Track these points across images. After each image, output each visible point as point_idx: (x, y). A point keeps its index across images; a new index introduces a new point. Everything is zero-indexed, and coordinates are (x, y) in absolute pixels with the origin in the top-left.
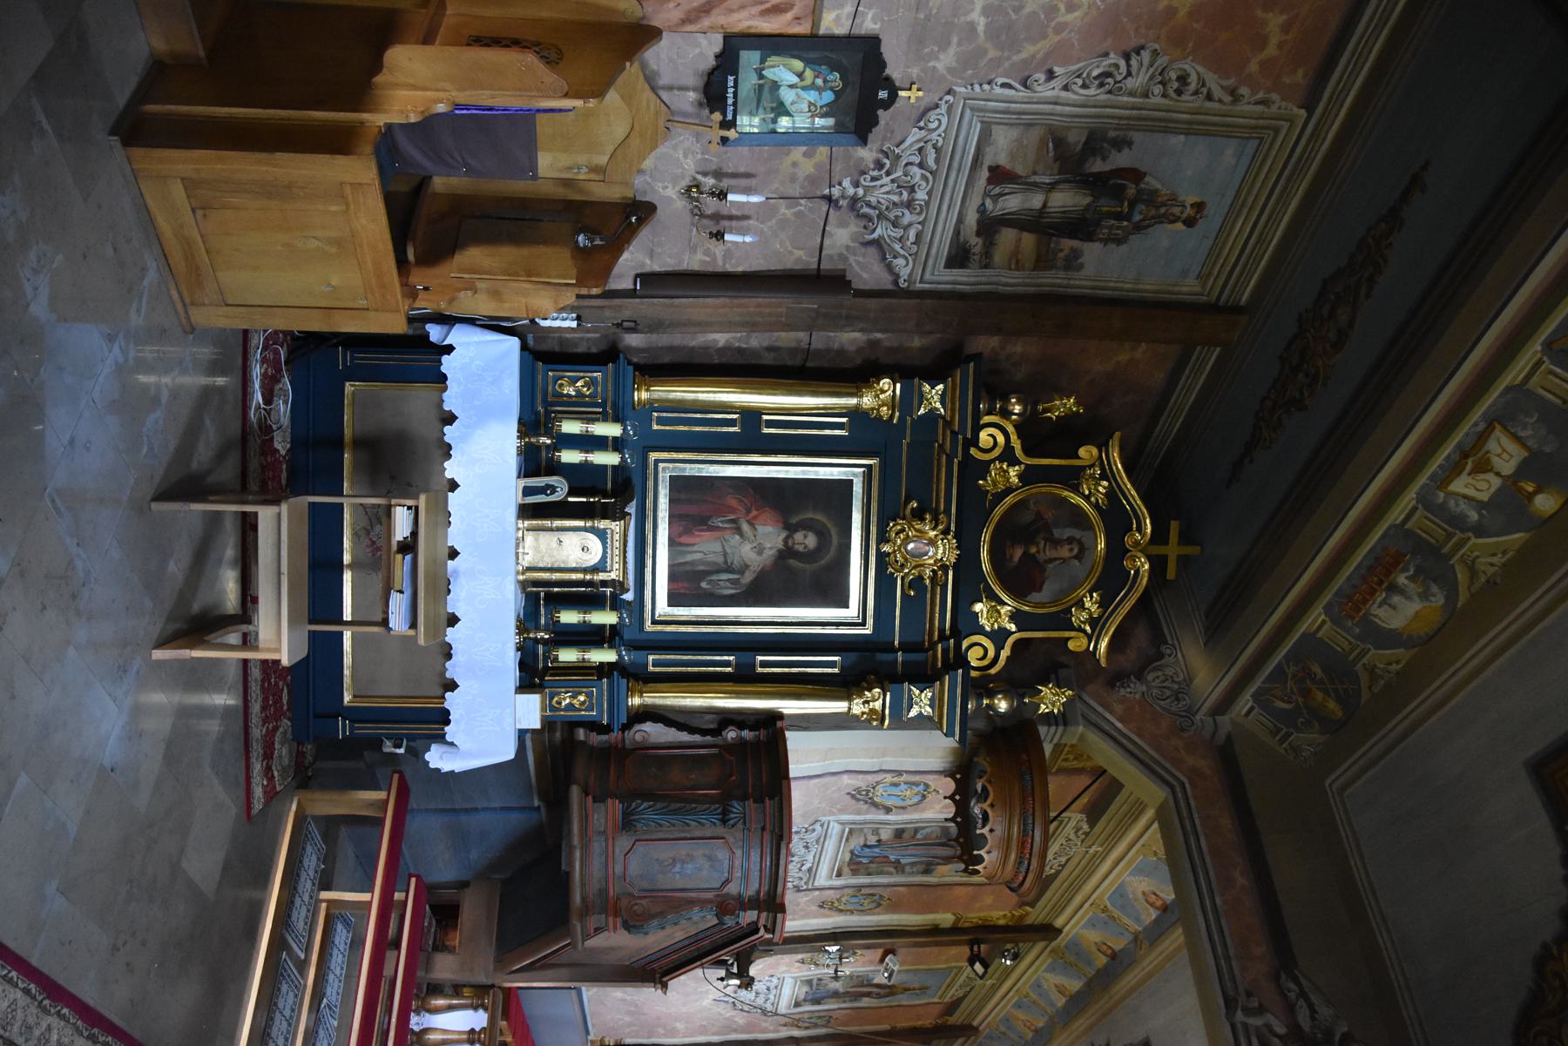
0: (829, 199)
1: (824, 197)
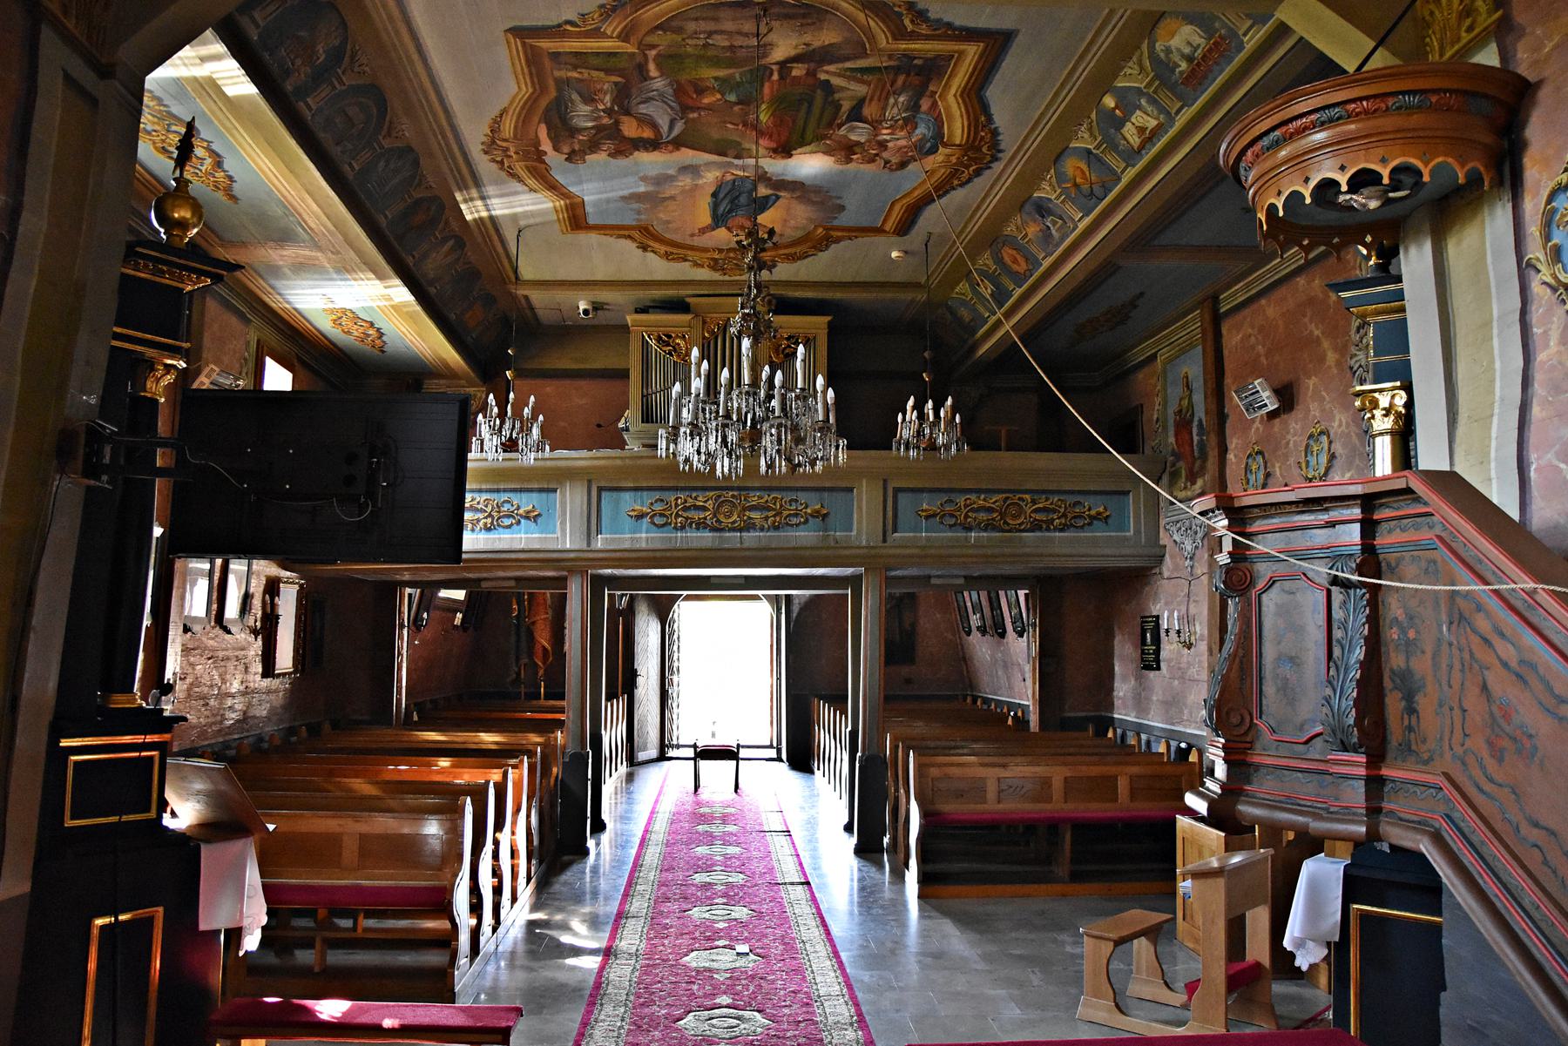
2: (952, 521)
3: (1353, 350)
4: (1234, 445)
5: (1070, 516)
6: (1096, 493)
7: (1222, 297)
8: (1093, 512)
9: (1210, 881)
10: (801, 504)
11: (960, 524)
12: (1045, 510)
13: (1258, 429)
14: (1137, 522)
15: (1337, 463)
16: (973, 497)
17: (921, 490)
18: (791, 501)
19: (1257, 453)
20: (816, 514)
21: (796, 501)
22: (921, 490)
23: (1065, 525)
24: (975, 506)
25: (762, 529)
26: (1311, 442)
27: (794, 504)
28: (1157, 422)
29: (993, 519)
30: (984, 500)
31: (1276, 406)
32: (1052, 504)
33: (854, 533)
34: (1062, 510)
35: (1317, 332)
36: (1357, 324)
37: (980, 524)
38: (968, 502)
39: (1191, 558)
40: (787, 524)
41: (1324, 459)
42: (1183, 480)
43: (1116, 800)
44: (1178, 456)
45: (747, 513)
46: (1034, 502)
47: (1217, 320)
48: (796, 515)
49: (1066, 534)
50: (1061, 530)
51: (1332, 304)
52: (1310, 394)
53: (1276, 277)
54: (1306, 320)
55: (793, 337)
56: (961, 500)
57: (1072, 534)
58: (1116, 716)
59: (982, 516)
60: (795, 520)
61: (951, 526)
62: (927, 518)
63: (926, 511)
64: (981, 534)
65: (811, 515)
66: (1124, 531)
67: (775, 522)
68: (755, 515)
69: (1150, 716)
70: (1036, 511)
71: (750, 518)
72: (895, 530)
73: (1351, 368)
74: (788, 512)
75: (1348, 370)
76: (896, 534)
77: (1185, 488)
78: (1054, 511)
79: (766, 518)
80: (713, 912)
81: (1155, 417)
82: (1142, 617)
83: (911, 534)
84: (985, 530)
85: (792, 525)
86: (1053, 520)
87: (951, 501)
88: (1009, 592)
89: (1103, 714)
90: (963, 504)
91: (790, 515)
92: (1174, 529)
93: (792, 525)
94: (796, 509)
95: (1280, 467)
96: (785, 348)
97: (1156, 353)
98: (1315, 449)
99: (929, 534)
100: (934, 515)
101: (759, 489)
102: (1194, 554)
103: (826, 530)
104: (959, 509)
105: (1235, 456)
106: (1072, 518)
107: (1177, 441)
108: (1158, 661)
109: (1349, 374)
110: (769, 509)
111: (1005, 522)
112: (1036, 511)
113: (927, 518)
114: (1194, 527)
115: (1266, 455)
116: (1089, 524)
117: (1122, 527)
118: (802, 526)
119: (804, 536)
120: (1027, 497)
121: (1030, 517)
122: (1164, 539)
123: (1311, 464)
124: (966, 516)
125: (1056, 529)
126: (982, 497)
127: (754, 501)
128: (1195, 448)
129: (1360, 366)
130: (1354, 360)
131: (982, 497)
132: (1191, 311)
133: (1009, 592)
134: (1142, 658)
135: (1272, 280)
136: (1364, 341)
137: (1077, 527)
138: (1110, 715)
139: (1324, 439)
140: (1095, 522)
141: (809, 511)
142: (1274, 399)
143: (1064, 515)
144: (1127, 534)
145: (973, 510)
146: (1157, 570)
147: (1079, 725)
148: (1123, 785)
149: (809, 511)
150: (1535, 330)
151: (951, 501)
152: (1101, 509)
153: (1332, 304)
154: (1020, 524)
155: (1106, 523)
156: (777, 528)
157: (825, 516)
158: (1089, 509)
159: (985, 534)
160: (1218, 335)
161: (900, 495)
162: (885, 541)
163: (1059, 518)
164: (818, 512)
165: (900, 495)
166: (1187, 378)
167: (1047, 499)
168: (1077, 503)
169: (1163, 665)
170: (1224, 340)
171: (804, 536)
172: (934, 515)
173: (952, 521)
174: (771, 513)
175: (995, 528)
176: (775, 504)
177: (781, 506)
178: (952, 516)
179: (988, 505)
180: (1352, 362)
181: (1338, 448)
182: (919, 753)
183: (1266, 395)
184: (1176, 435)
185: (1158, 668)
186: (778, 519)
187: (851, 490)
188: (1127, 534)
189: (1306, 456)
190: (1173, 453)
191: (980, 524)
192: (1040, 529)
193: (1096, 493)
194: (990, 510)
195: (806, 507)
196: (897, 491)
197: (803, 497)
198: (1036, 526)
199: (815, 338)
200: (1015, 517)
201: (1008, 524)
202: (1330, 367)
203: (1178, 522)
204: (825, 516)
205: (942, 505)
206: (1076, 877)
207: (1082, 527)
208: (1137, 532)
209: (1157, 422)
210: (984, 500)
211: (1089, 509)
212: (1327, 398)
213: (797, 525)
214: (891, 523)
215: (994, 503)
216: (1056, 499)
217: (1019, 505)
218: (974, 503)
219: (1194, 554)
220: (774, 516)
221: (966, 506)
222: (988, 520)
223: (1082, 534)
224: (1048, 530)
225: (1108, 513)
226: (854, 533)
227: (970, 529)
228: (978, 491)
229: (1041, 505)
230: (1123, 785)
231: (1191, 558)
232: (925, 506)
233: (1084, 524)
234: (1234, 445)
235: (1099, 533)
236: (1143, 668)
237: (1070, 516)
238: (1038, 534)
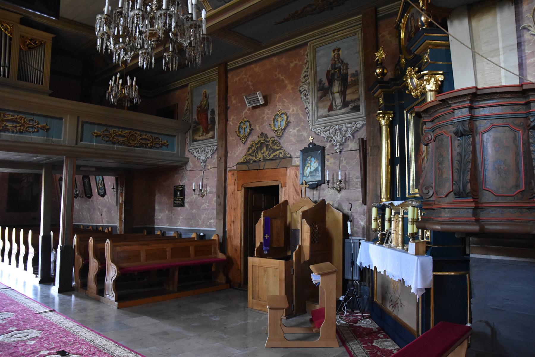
0: (340, 152)
1: (340, 154)
2: (107, 139)
3: (301, 84)
4: (231, 119)
5: (154, 143)
6: (164, 135)
7: (228, 63)
8: (162, 142)
9: (329, 276)
10: (36, 122)
11: (111, 141)
12: (145, 139)
13: (246, 113)
14: (178, 148)
15: (291, 125)
16: (117, 130)
17: (94, 124)
18: (30, 120)
19: (246, 122)
20: (43, 128)
21: (33, 120)
22: (94, 124)
23: (152, 146)
24: (118, 134)
25: (13, 132)
26: (242, 125)
27: (31, 121)
28: (186, 111)
29: (125, 141)
30: (121, 132)
31: (263, 103)
32: (148, 137)
33: (62, 139)
34: (151, 140)
35: (282, 78)
36: (304, 75)
37: (119, 142)
38: (115, 131)
39: (204, 162)
40: (27, 131)
41: (248, 130)
42: (201, 132)
43: (190, 256)
44: (197, 123)
45: (5, 123)
46: (141, 135)
47: (226, 72)
48: (32, 127)
49: (152, 150)
50: (151, 148)
51: (291, 67)
52: (277, 99)
53: (261, 57)
54: (277, 73)
55: (34, 40)
56: (112, 130)
57: (155, 150)
58: (155, 226)
59: (120, 139)
60: (31, 130)
61: (107, 141)
62: (96, 136)
63: (96, 133)
64: (119, 146)
65: (41, 129)
66: (173, 151)
67: (20, 129)
68: (9, 125)
69: (178, 225)
70: (141, 139)
71: (5, 125)
72: (82, 140)
73: (300, 91)
74: (28, 125)
75: (298, 91)
76: (82, 142)
77: (202, 135)
78: (148, 140)
79: (16, 127)
80: (16, 336)
81: (186, 108)
82: (174, 186)
83: (89, 143)
84: (121, 145)
85: (30, 132)
86: (148, 144)
87: (107, 130)
88: (97, 177)
89: (148, 226)
90: (112, 132)
91: (29, 127)
92: (195, 151)
93: (30, 132)
94: (33, 124)
95: (259, 127)
96: (28, 44)
97: (188, 84)
98: (279, 119)
99: (97, 144)
100: (100, 136)
101: (12, 111)
102: (206, 161)
103: (47, 137)
104: (111, 135)
105: (233, 123)
106: (155, 144)
107: (198, 118)
108: (183, 203)
109: (299, 93)
110: (17, 122)
111: (129, 143)
112: (141, 139)
113: (96, 136)
114: (206, 150)
115: (251, 122)
116: (161, 147)
117: (173, 150)
118: (35, 133)
119: (36, 138)
120: (138, 133)
121: (139, 141)
122: (187, 155)
123: (277, 125)
124: (113, 138)
125: (149, 148)
126: (121, 130)
127: (9, 116)
128: (209, 120)
129: (305, 90)
130: (302, 88)
131: (121, 130)
132: (215, 66)
133: (97, 177)
134: (174, 203)
135: (258, 58)
136: (307, 81)
137: (156, 148)
138: (153, 226)
139: (284, 116)
140: (163, 146)
141: (40, 126)
142: (263, 100)
143: (152, 142)
144: (174, 152)
145: (116, 135)
146: (184, 168)
147: (140, 230)
148: (143, 255)
149: (40, 126)
150: (527, 51)
151: (107, 130)
152: (166, 142)
153: (291, 67)
154: (135, 144)
155: (167, 147)
156: (21, 133)
157: (48, 130)
158: (161, 141)
159: (121, 147)
160: (227, 77)
161: (85, 125)
162: (76, 144)
163: (150, 143)
164: (44, 127)
165: (85, 125)
166: (206, 93)
167: (146, 135)
168: (157, 138)
169: (186, 204)
170: (229, 80)
171: (36, 138)
172: (100, 136)
173: (107, 139)
174: (18, 125)
175: (125, 145)
176: (21, 120)
177: (24, 122)
178: (107, 137)
179: (123, 134)
180: (301, 89)
181: (291, 119)
182: (112, 241)
183: (260, 98)
184: (198, 115)
185: (184, 206)
186: (22, 128)
187: (62, 119)
188: (174, 152)
189: (274, 122)
190: (195, 122)
191: (119, 142)
192: (143, 147)
193: (164, 135)
194: (124, 136)
195: (38, 124)
196: (83, 123)
197: (36, 119)
198: (141, 146)
199: (45, 43)
200: (133, 141)
201: (130, 143)
202: (288, 90)
203: (197, 148)
204: (48, 130)
205: (103, 131)
206: (181, 289)
207: (158, 148)
208: (178, 152)
209: (186, 111)
210: (121, 132)
211: (161, 141)
212: (286, 101)
213: (33, 132)
214: (80, 137)
215: (125, 134)
216: (149, 135)
217: (135, 136)
218: (117, 133)
219: (206, 161)
220: (20, 126)
221: (114, 133)
222: (122, 141)
223: (158, 151)
224: (146, 147)
225: (168, 143)
226: (62, 139)
227: (114, 144)
228: (119, 128)
229: (144, 137)
230: (143, 255)
231: (204, 162)
232: (96, 131)
233: (159, 147)
234: (231, 119)
235: (164, 151)
236: (174, 206)
237: (154, 143)
238: (141, 149)
